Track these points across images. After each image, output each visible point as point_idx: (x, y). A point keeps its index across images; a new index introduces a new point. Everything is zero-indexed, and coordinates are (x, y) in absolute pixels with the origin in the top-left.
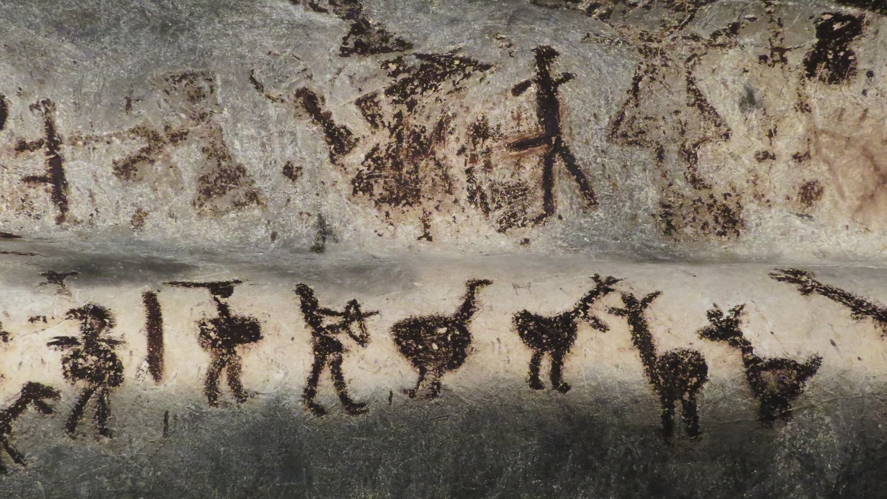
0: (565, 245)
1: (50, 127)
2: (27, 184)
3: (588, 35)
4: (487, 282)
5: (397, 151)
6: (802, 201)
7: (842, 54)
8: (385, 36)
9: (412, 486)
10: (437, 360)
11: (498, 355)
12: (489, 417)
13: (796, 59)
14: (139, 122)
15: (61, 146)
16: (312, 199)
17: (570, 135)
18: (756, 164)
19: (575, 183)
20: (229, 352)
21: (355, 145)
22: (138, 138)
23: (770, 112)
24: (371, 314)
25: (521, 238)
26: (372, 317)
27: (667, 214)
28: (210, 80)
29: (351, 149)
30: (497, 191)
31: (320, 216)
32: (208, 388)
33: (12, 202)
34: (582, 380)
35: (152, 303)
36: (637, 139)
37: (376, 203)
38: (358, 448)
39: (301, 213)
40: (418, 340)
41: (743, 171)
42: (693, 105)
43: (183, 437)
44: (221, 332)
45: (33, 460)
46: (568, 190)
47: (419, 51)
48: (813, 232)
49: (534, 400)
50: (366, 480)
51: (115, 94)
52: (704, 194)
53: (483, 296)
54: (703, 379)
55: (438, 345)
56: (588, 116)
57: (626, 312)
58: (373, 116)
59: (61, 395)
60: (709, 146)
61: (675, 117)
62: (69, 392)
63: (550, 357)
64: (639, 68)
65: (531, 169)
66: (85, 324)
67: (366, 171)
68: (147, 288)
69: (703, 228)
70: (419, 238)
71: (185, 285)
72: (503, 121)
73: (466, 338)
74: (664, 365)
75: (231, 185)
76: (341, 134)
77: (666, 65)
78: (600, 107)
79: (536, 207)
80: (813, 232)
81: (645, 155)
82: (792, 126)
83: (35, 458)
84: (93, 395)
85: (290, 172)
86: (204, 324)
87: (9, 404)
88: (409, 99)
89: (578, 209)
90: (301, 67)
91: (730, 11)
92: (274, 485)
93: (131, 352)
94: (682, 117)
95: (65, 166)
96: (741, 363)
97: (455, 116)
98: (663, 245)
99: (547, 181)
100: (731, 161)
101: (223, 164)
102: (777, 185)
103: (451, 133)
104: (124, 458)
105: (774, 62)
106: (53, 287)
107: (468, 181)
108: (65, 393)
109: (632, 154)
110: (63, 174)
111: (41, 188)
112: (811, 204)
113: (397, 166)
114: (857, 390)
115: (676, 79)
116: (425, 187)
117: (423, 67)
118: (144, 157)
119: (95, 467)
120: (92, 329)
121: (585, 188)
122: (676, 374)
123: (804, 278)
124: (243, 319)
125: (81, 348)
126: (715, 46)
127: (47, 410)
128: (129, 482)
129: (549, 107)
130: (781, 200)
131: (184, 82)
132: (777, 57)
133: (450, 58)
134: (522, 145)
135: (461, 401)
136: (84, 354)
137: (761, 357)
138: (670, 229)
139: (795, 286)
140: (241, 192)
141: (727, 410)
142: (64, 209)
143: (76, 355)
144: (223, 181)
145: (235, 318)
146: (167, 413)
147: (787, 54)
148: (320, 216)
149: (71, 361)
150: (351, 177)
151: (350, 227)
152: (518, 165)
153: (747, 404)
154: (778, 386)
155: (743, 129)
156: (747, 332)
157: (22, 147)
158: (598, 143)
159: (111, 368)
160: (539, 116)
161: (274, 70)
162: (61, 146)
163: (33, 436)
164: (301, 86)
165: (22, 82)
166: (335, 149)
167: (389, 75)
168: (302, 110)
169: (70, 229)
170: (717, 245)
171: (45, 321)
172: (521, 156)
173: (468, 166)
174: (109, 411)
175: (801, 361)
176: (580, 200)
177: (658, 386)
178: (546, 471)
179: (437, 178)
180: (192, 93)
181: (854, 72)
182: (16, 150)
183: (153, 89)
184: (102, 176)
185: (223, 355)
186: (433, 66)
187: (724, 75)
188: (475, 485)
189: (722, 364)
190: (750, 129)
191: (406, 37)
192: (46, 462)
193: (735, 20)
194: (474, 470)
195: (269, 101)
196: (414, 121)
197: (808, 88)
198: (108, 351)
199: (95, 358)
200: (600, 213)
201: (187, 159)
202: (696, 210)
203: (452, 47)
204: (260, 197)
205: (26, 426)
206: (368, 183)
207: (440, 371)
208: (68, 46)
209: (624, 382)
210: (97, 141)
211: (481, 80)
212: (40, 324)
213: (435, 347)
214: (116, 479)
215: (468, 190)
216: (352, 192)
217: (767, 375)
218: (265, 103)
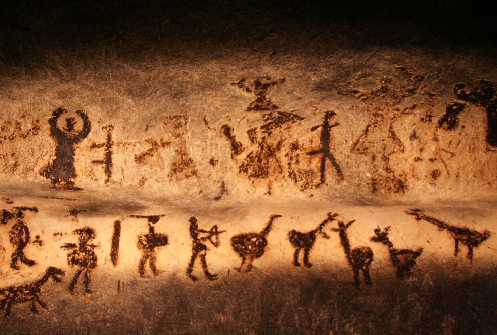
0: (328, 197)
1: (109, 138)
2: (93, 164)
3: (353, 106)
4: (280, 216)
5: (260, 154)
6: (432, 178)
7: (453, 119)
8: (269, 103)
9: (242, 313)
10: (251, 253)
11: (280, 250)
12: (275, 281)
13: (435, 120)
14: (150, 137)
15: (112, 147)
16: (220, 175)
17: (334, 149)
18: (414, 163)
19: (334, 170)
20: (151, 251)
21: (243, 151)
22: (148, 144)
23: (422, 141)
24: (222, 232)
25: (310, 194)
26: (223, 233)
27: (374, 183)
28: (186, 119)
29: (241, 152)
30: (300, 173)
31: (223, 183)
32: (140, 269)
33: (85, 172)
34: (317, 262)
35: (117, 226)
36: (364, 151)
37: (249, 177)
38: (214, 296)
39: (215, 181)
40: (243, 244)
41: (408, 165)
42: (391, 137)
43: (128, 293)
44: (149, 241)
45: (52, 306)
46: (331, 173)
47: (279, 110)
48: (436, 191)
49: (296, 271)
50: (219, 312)
51: (142, 123)
52: (391, 175)
53: (276, 223)
54: (371, 260)
55: (252, 247)
56: (342, 141)
57: (339, 230)
58: (253, 138)
59: (66, 273)
60: (395, 155)
61: (382, 143)
62: (70, 271)
63: (303, 252)
64: (371, 121)
65: (316, 162)
66: (81, 237)
67: (246, 163)
68: (118, 218)
69: (389, 190)
70: (265, 194)
71: (138, 217)
72: (305, 142)
73: (265, 243)
74: (354, 254)
75: (186, 167)
76: (238, 146)
77: (382, 121)
78: (349, 137)
79: (317, 180)
80: (436, 191)
81: (367, 158)
82: (430, 147)
83: (52, 305)
84: (82, 273)
85: (212, 162)
86: (141, 237)
87: (39, 278)
88: (269, 131)
89: (335, 182)
90: (226, 115)
91: (415, 99)
92: (174, 316)
93: (102, 252)
94: (385, 142)
95: (112, 156)
96: (388, 252)
97: (285, 139)
98: (370, 197)
99: (323, 169)
100: (404, 161)
101: (184, 157)
102: (422, 171)
103: (283, 147)
104: (98, 304)
105: (426, 121)
106: (72, 217)
107: (289, 168)
108: (68, 272)
109: (361, 157)
110: (111, 160)
111: (100, 166)
112: (435, 179)
113: (260, 161)
114: (440, 261)
115: (386, 126)
116: (271, 170)
117: (279, 117)
118: (149, 153)
119: (84, 309)
120: (84, 239)
121: (339, 171)
122: (359, 258)
123: (419, 213)
124: (160, 235)
125: (77, 249)
126: (404, 114)
127: (59, 280)
128: (101, 316)
129: (326, 136)
130: (423, 177)
131: (174, 119)
132: (428, 119)
133: (290, 114)
134: (312, 153)
135: (262, 273)
136: (79, 252)
137: (397, 249)
138: (374, 190)
139: (414, 217)
140: (190, 171)
141: (383, 273)
142: (109, 176)
143: (75, 253)
144: (182, 166)
145: (156, 234)
146: (119, 281)
147: (432, 118)
148: (223, 183)
149: (71, 256)
150: (239, 165)
151: (235, 188)
152: (310, 162)
153: (391, 270)
154: (404, 261)
155: (410, 148)
156: (391, 238)
157: (94, 146)
158: (346, 153)
159: (91, 259)
160: (321, 141)
161: (214, 116)
162: (112, 147)
163: (51, 294)
164: (225, 123)
165: (102, 116)
166: (234, 152)
167: (264, 120)
168: (223, 134)
169: (110, 186)
170: (394, 197)
171: (61, 235)
172: (311, 158)
173: (289, 162)
174: (90, 281)
175: (414, 250)
176: (336, 177)
177: (351, 263)
178: (305, 303)
179: (276, 167)
180: (177, 125)
181: (457, 126)
182: (91, 147)
183: (160, 122)
184: (129, 161)
185: (148, 252)
186: (282, 117)
187: (405, 126)
188: (272, 311)
189: (380, 252)
190: (413, 148)
191: (277, 104)
192: (58, 307)
193: (415, 104)
194: (271, 304)
195: (209, 130)
196: (269, 141)
197: (438, 132)
198: (91, 251)
199: (84, 254)
200: (345, 183)
201: (168, 155)
202: (387, 182)
203: (293, 109)
204: (197, 173)
205: (47, 289)
206: (246, 168)
207: (252, 259)
208: (130, 101)
209: (336, 262)
210: (129, 145)
211: (299, 124)
212: (59, 236)
213: (250, 247)
214: (94, 315)
215: (289, 172)
216: (238, 171)
217: (399, 257)
218: (207, 130)
